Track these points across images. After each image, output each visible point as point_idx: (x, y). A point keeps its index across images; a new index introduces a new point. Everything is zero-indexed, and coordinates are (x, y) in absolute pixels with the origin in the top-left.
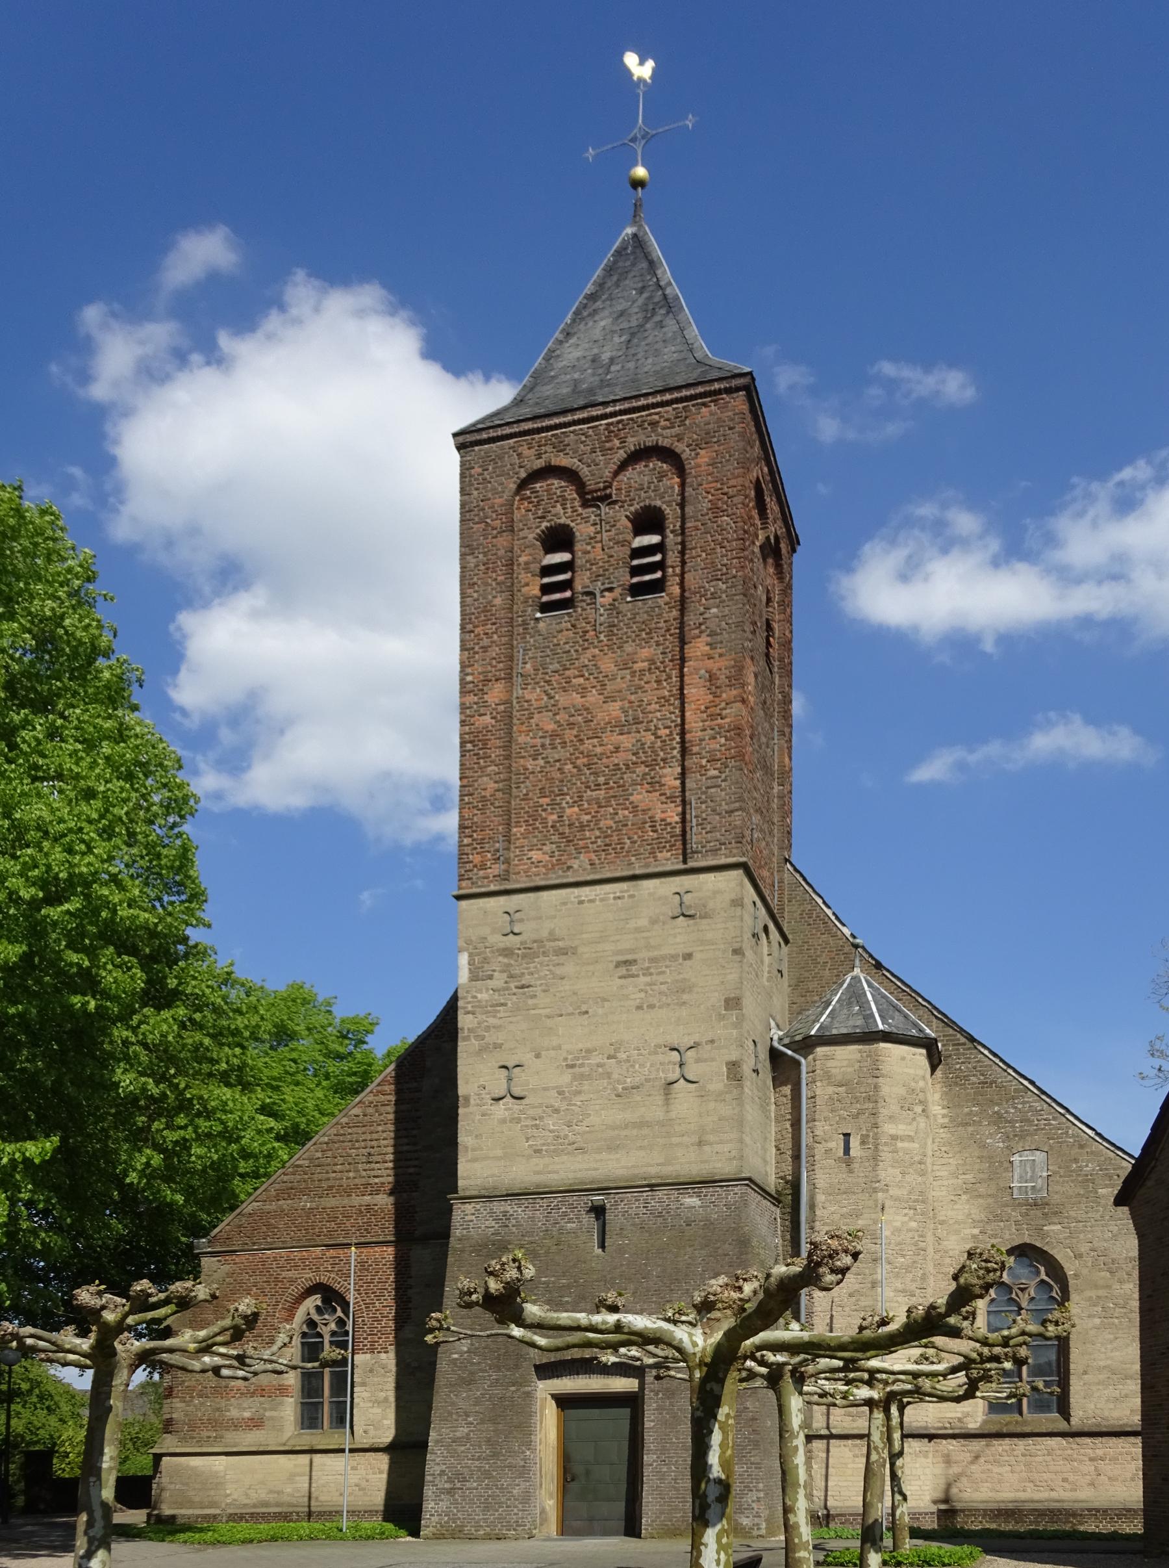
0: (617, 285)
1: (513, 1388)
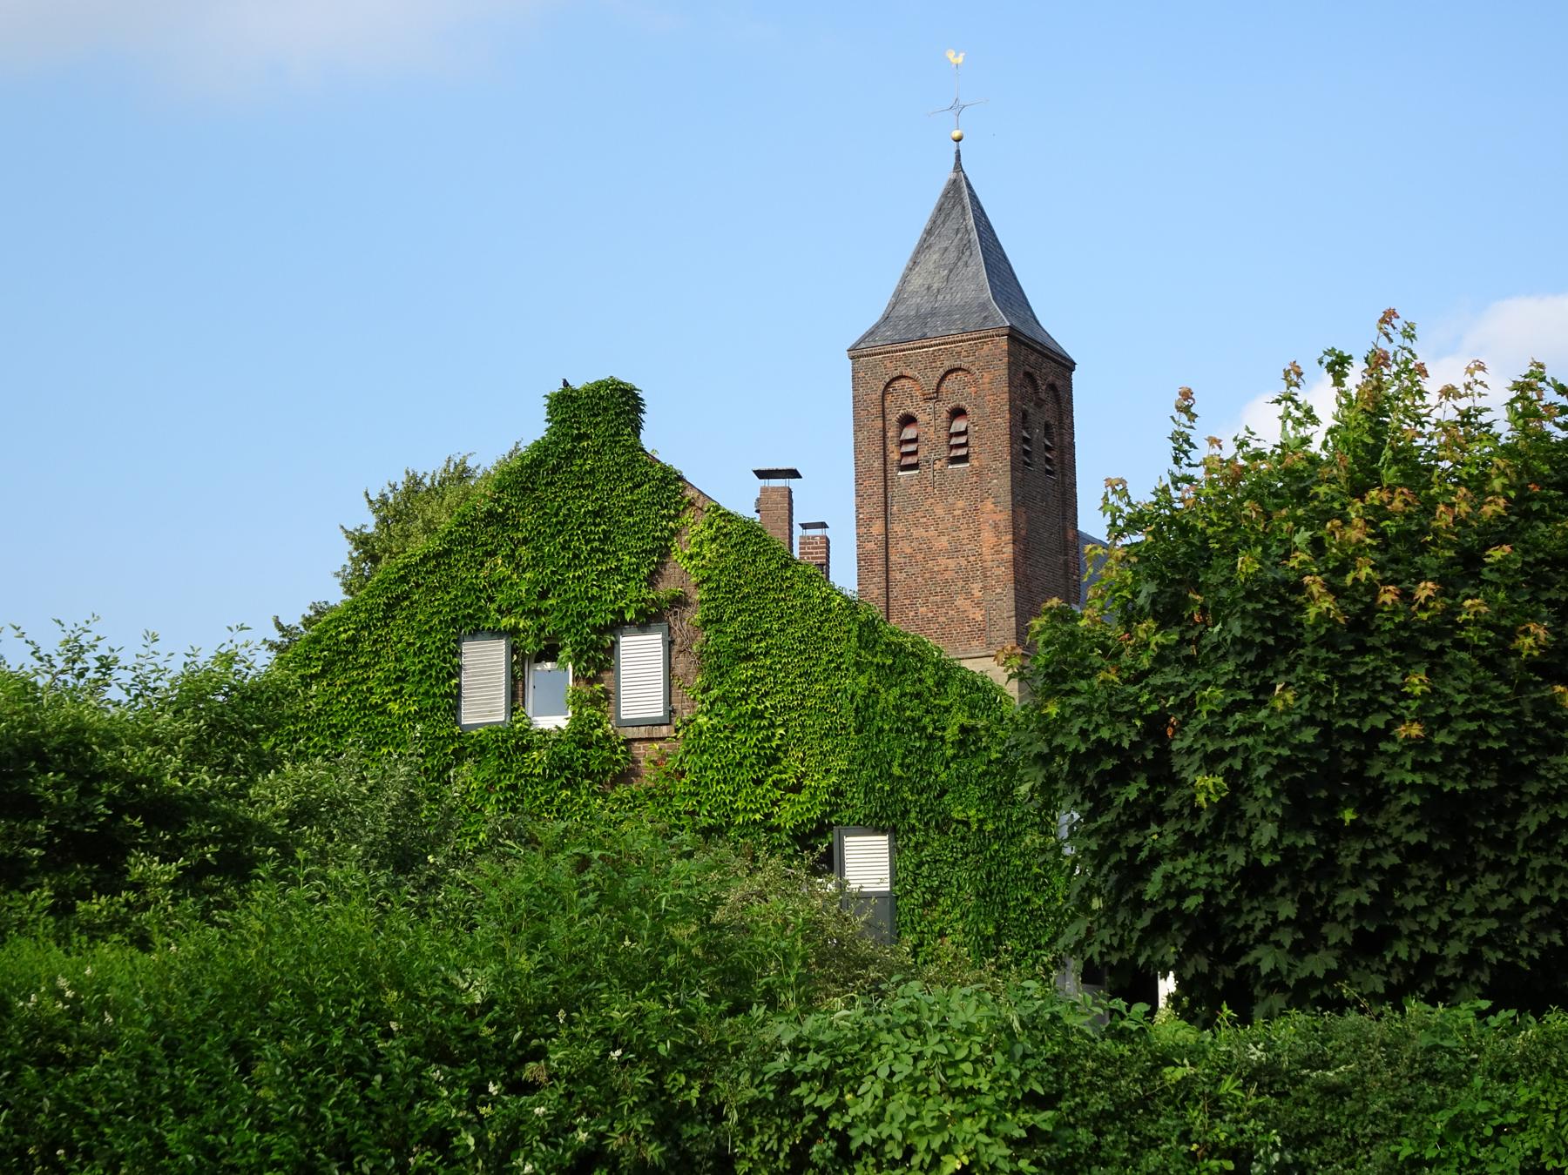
0: (943, 223)
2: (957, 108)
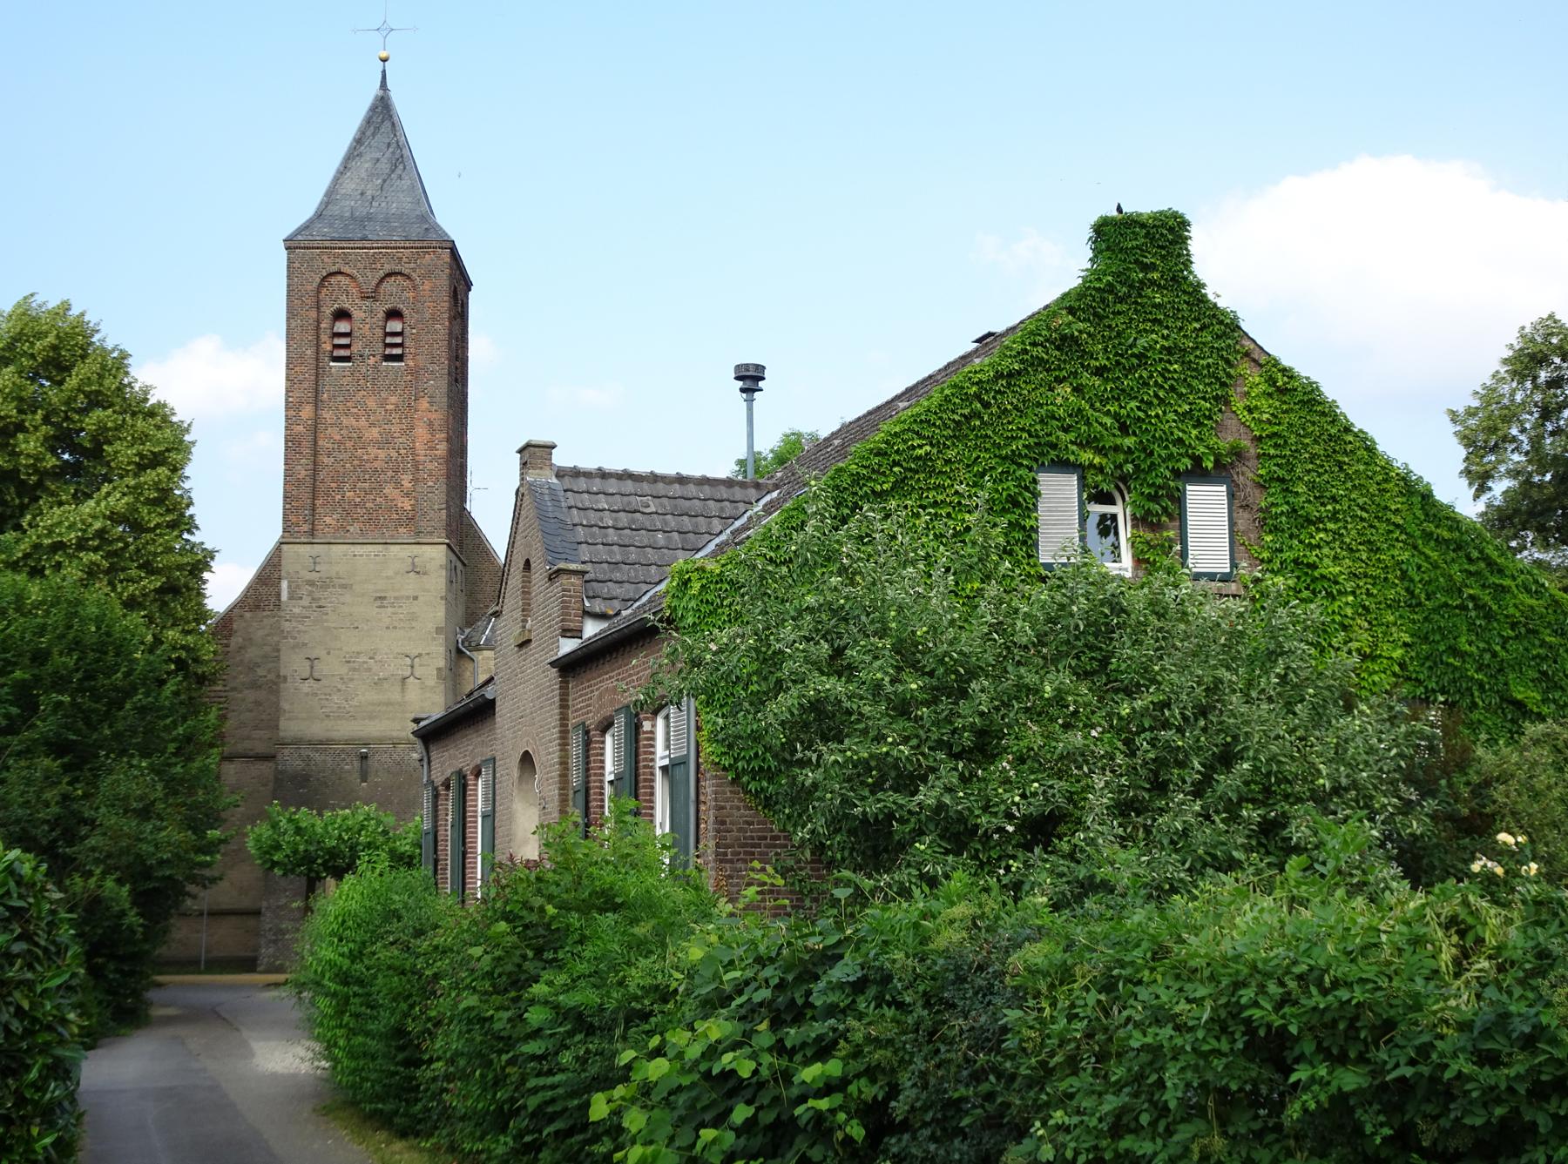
0: (374, 135)
2: (385, 30)
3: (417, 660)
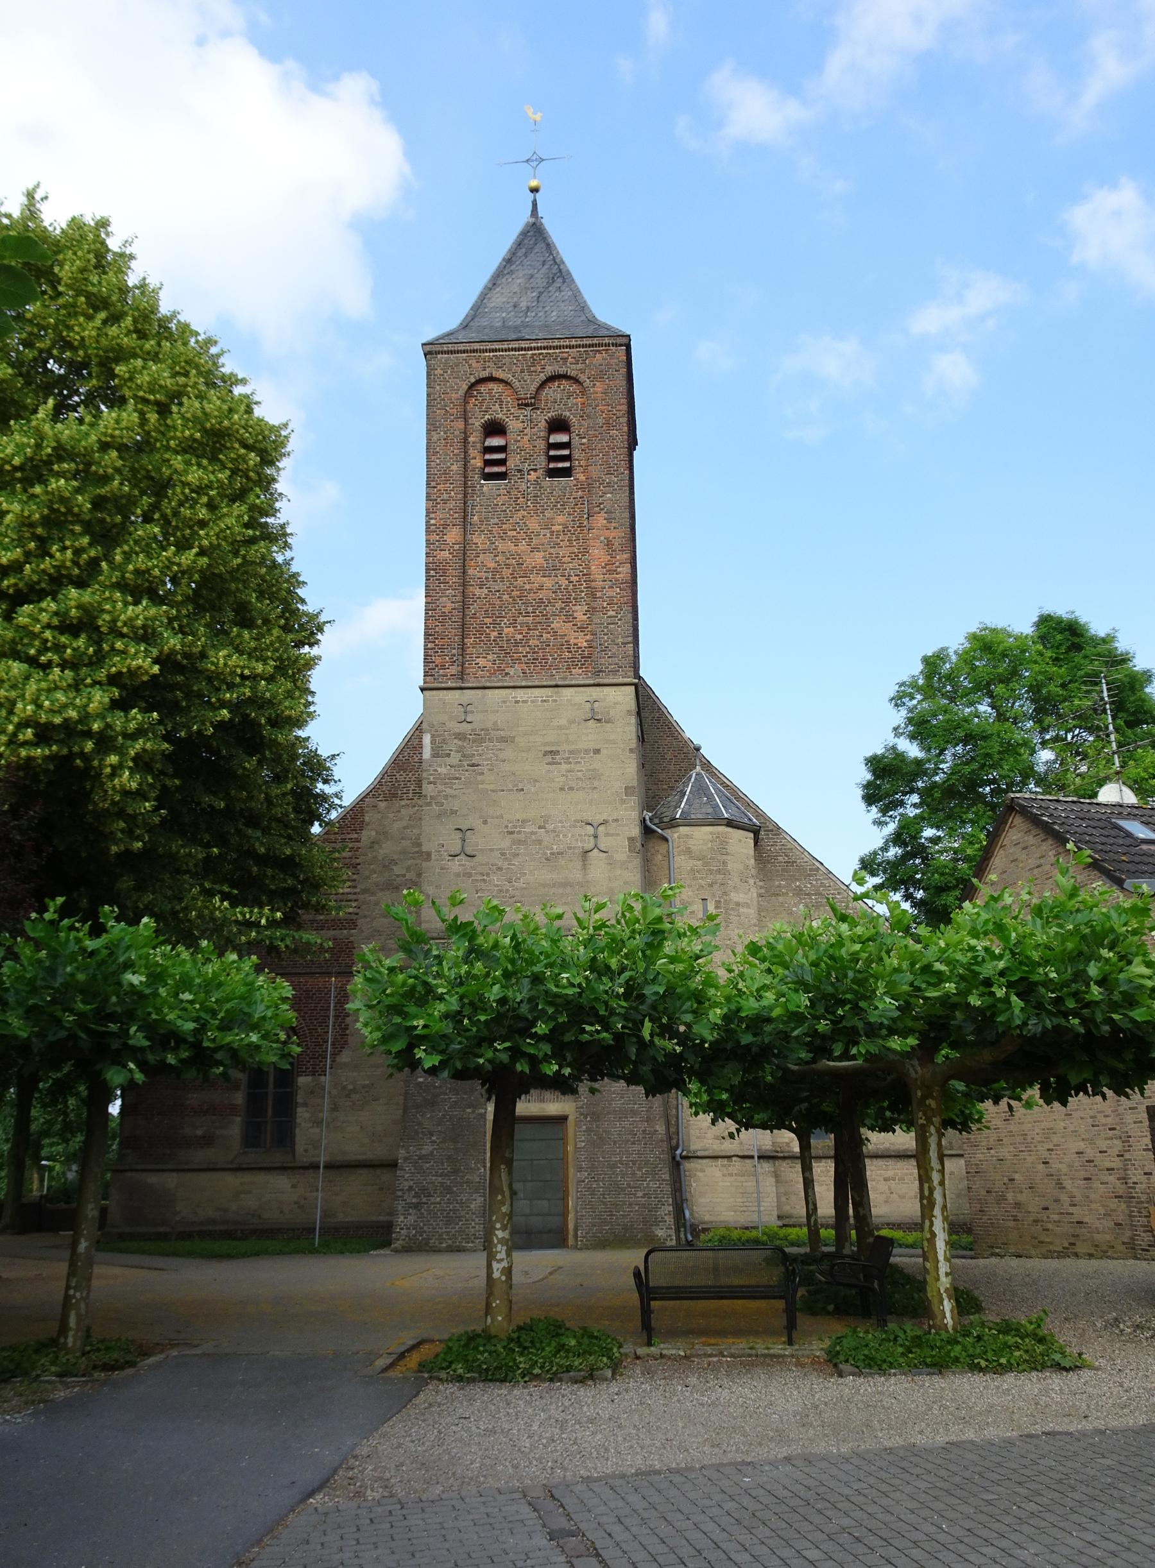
0: (526, 255)
1: (469, 1110)
3: (601, 828)
